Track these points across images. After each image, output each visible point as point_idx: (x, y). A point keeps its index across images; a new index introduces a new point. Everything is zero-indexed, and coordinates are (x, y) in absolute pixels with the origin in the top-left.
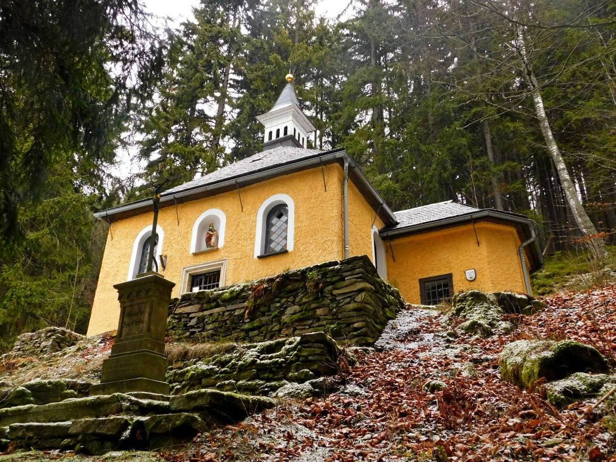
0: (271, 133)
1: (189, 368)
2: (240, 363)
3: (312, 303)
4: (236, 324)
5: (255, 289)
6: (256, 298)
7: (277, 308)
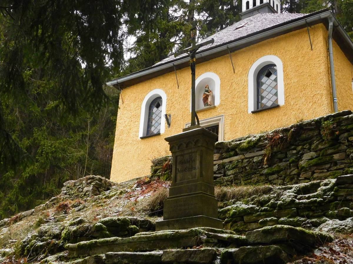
0: (248, 3)
1: (229, 207)
2: (279, 202)
3: (328, 149)
4: (255, 169)
5: (271, 139)
6: (272, 147)
7: (294, 154)
